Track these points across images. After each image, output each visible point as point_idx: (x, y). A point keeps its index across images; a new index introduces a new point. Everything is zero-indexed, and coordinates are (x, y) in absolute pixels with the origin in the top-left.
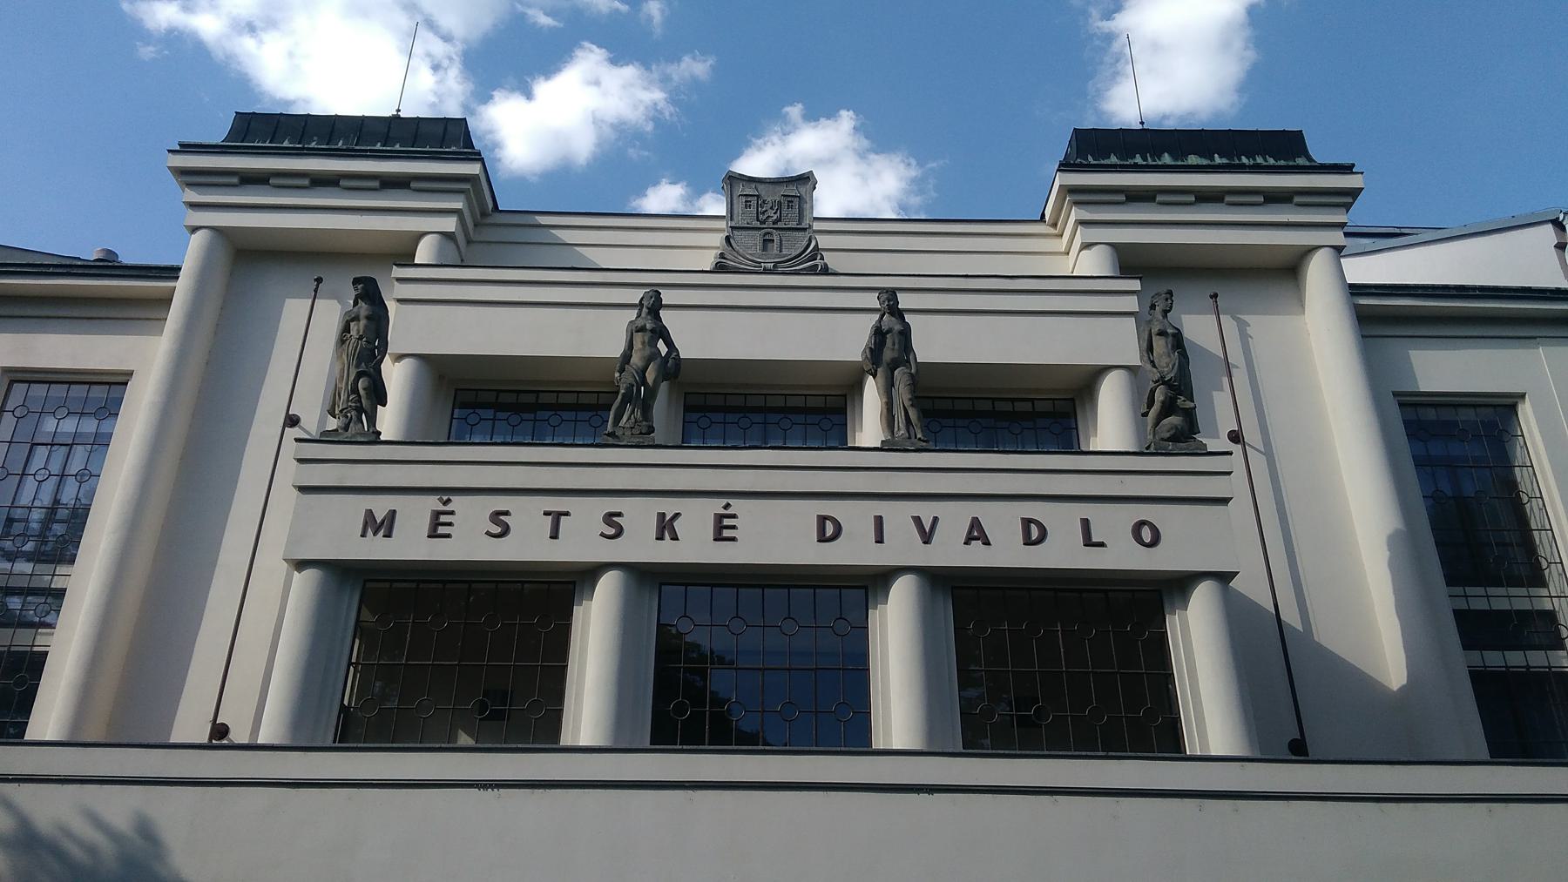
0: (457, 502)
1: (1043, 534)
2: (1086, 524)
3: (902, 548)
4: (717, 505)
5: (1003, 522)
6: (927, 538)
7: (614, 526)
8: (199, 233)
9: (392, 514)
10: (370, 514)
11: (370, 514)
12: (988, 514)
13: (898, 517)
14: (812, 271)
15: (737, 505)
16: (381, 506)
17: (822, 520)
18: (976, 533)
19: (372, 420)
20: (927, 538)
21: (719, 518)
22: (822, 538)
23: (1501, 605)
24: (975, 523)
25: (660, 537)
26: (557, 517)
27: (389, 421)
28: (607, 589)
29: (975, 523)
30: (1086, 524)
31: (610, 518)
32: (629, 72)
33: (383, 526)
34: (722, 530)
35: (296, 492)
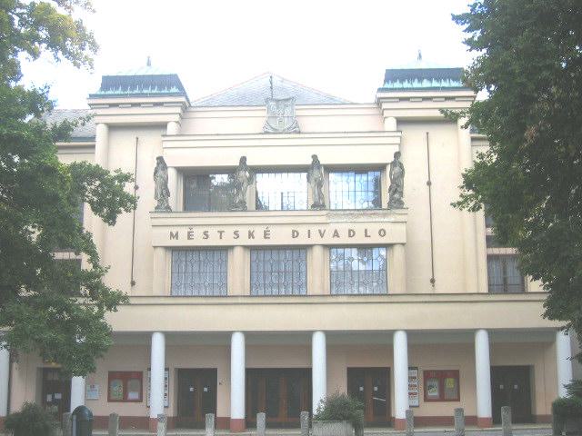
0: (194, 229)
1: (298, 234)
2: (366, 231)
3: (316, 239)
4: (264, 228)
5: (213, 232)
6: (322, 236)
7: (237, 234)
8: (100, 125)
9: (177, 233)
10: (171, 234)
11: (171, 234)
12: (300, 229)
13: (314, 230)
14: (296, 132)
15: (271, 228)
16: (174, 230)
17: (293, 232)
18: (251, 235)
19: (167, 201)
20: (322, 236)
21: (189, 233)
22: (350, 236)
23: (497, 249)
24: (336, 231)
25: (334, 236)
26: (221, 232)
27: (172, 201)
28: (238, 252)
29: (336, 231)
30: (366, 231)
31: (236, 233)
32: (94, 164)
33: (175, 236)
34: (266, 235)
35: (457, 210)
